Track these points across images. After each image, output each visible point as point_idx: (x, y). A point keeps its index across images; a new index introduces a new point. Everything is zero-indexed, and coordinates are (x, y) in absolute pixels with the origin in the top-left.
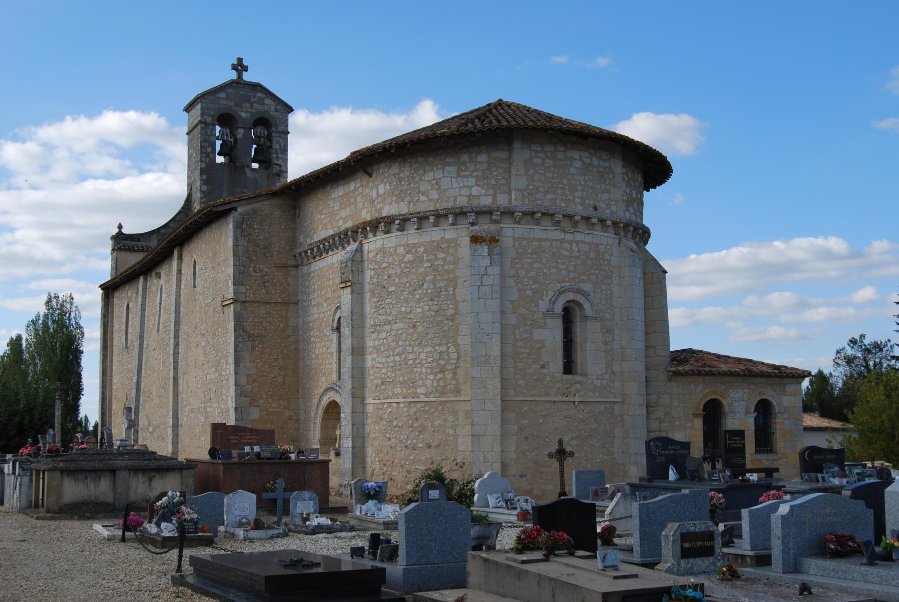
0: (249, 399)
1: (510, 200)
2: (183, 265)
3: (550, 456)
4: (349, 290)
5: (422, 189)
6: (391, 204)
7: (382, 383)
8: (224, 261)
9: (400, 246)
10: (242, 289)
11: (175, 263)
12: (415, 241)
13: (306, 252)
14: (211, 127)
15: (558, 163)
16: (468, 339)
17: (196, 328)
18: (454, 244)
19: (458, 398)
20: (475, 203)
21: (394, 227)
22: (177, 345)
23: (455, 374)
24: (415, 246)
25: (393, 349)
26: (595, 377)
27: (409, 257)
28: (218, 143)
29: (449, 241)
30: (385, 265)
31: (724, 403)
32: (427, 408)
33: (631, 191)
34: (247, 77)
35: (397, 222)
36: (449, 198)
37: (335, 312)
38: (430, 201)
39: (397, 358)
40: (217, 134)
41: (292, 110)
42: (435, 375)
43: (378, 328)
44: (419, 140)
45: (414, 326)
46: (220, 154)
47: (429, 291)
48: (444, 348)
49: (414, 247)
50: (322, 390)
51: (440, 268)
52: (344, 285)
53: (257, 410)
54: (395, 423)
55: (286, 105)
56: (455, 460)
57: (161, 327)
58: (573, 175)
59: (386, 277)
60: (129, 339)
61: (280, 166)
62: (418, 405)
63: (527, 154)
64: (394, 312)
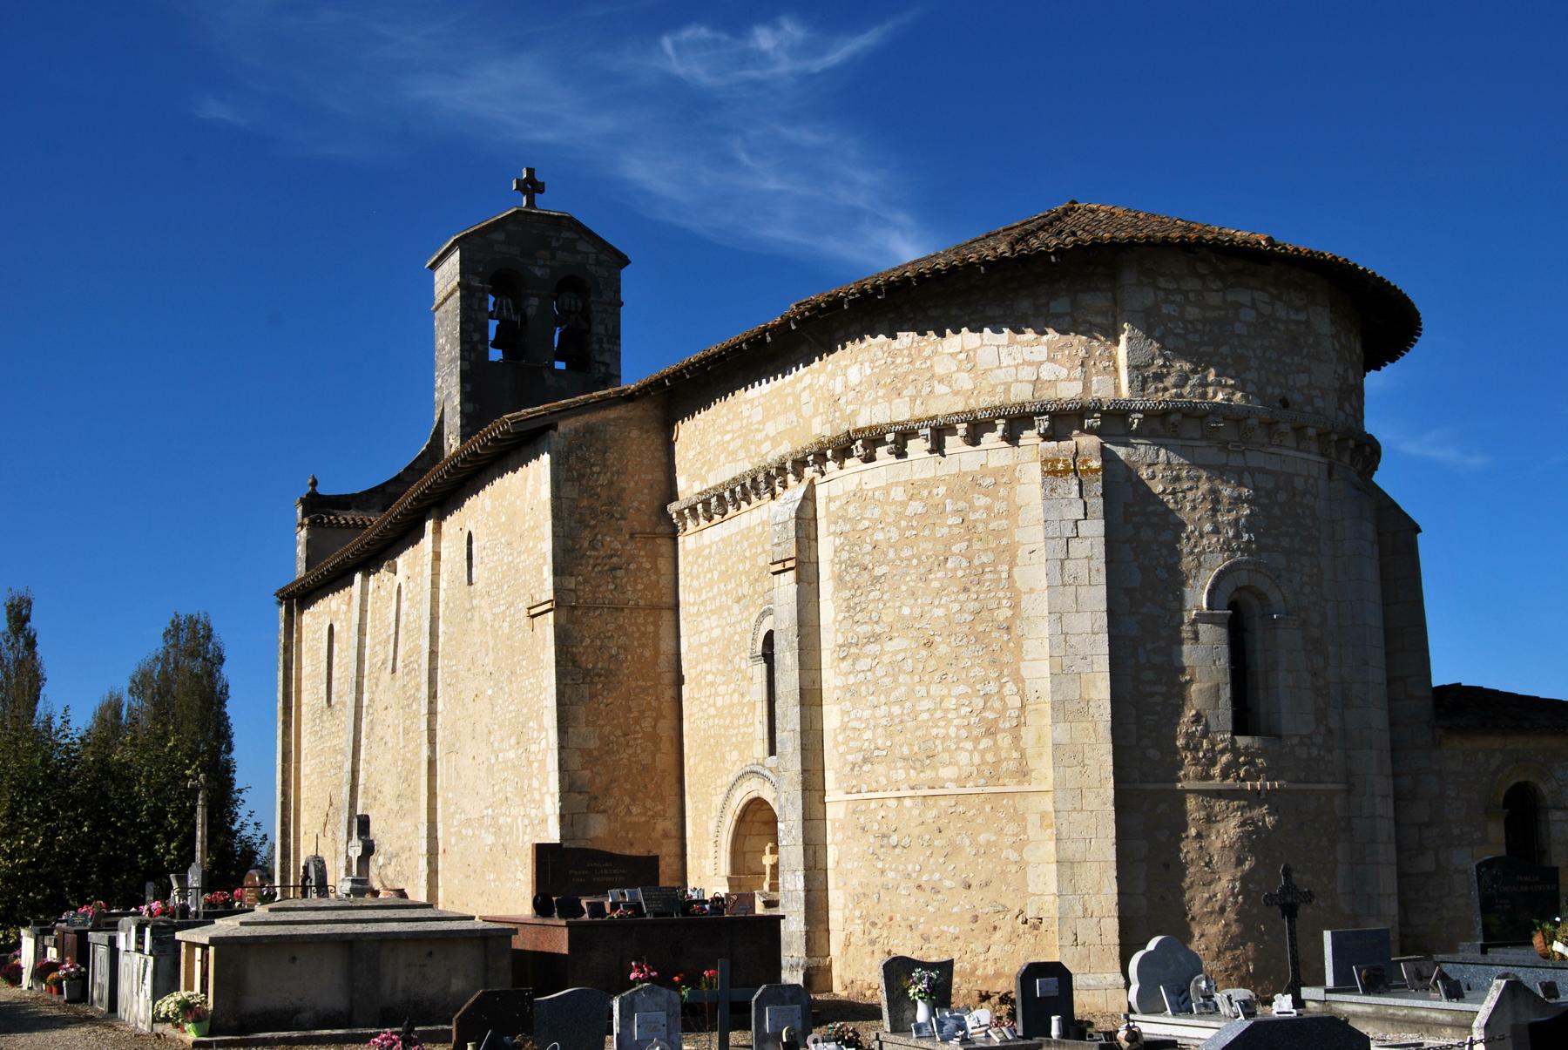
0: (587, 797)
1: (1117, 388)
2: (443, 544)
3: (1309, 897)
4: (791, 575)
5: (939, 370)
6: (875, 402)
7: (865, 760)
8: (533, 529)
9: (897, 484)
10: (571, 583)
11: (427, 541)
12: (928, 474)
13: (693, 509)
14: (479, 295)
15: (1210, 314)
16: (1044, 668)
17: (473, 661)
18: (1006, 478)
19: (1026, 788)
20: (1048, 394)
21: (881, 452)
22: (433, 697)
23: (1017, 738)
24: (926, 484)
25: (887, 693)
26: (1295, 741)
27: (916, 507)
28: (493, 325)
29: (998, 472)
30: (866, 523)
31: (1545, 789)
32: (960, 809)
33: (1346, 370)
34: (547, 204)
35: (890, 437)
36: (994, 387)
37: (759, 622)
38: (956, 393)
39: (896, 710)
40: (491, 308)
41: (627, 262)
42: (977, 740)
43: (853, 650)
44: (936, 272)
45: (929, 644)
46: (495, 345)
47: (960, 573)
48: (993, 687)
49: (926, 486)
50: (732, 778)
51: (981, 528)
52: (779, 567)
53: (601, 818)
54: (894, 839)
55: (617, 253)
56: (1021, 912)
57: (399, 664)
58: (1239, 336)
59: (869, 548)
60: (334, 690)
61: (607, 365)
62: (943, 803)
63: (1148, 298)
64: (888, 617)
